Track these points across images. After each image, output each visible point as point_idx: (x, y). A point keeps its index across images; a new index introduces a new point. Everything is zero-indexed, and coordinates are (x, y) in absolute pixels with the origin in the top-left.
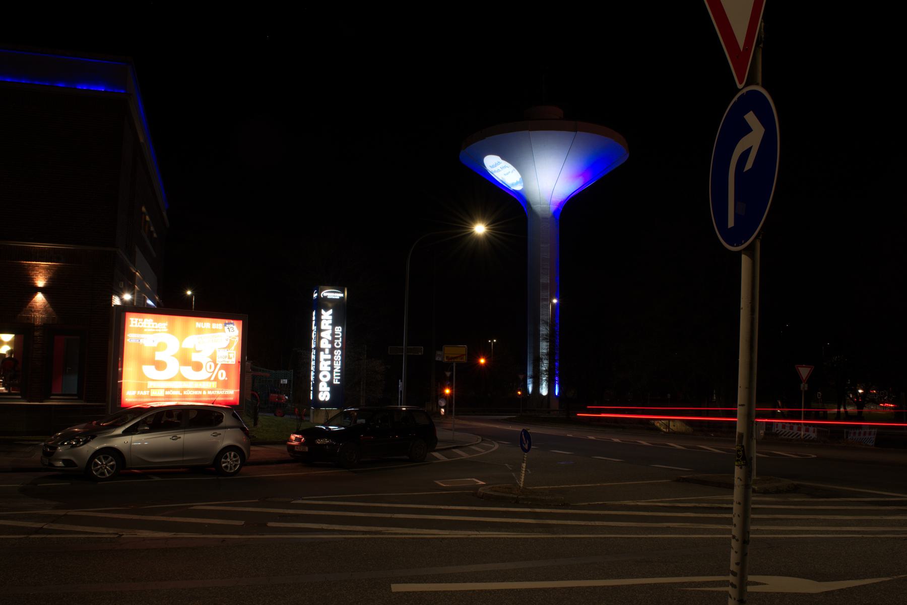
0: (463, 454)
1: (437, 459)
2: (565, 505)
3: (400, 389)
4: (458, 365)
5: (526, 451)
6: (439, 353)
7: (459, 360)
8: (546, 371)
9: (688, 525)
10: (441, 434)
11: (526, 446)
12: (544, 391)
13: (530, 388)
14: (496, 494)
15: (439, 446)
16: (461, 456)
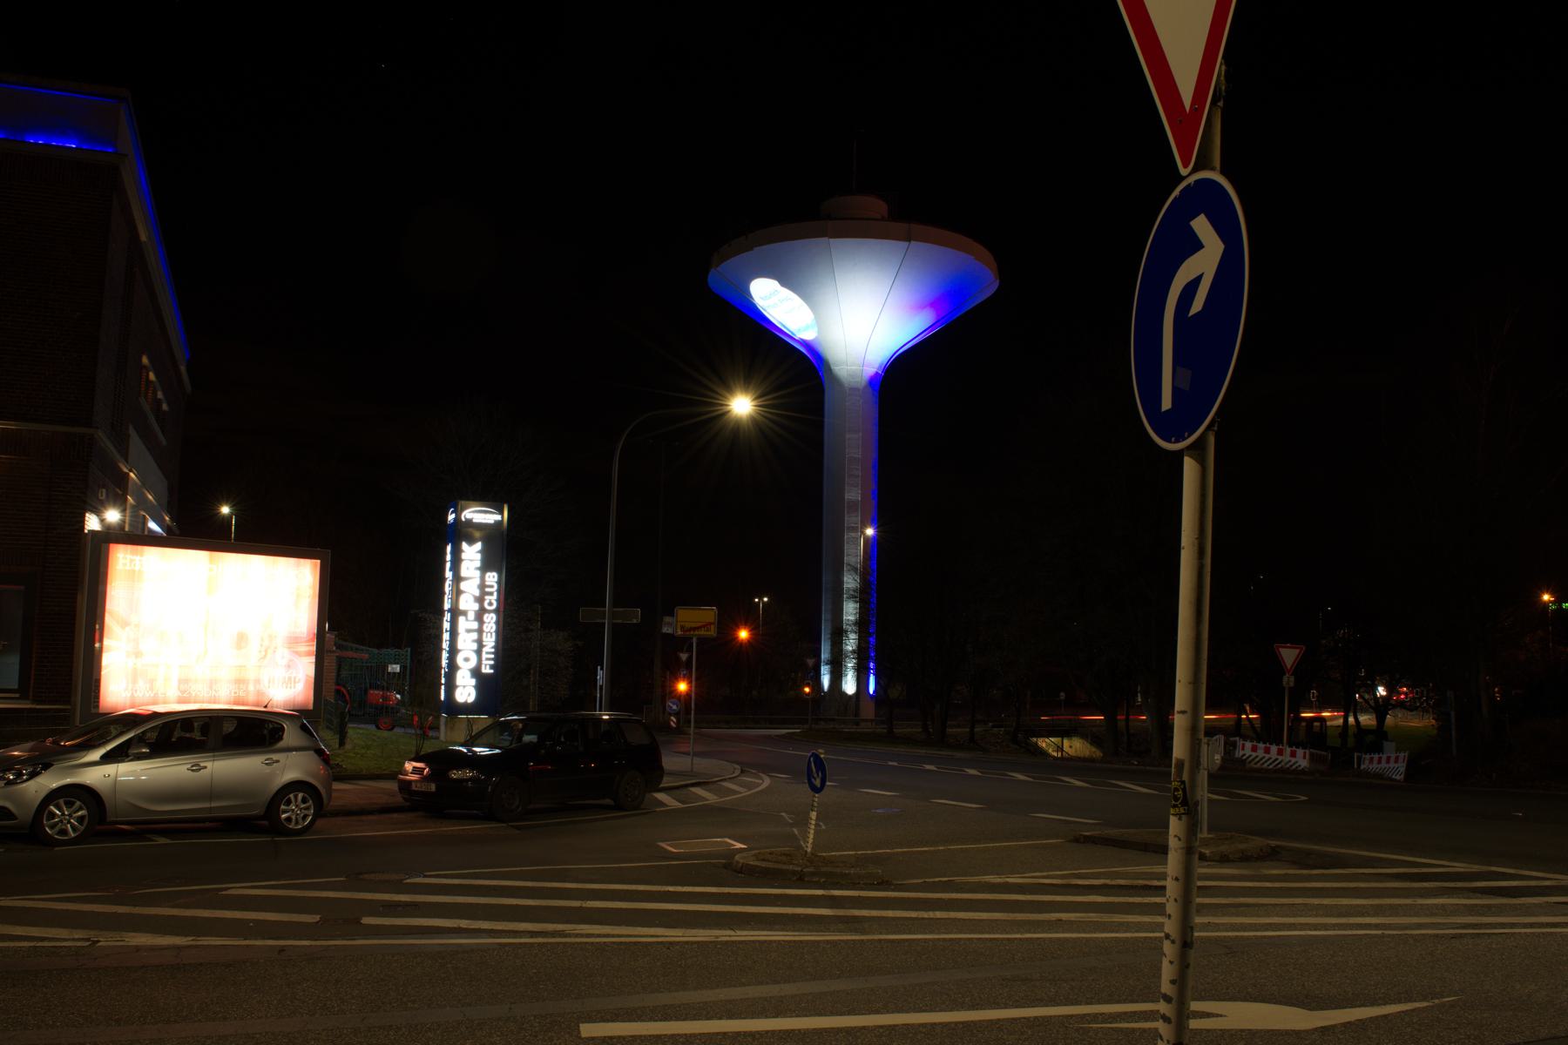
0: (708, 796)
1: (662, 804)
2: (883, 884)
3: (600, 682)
4: (702, 641)
5: (816, 790)
6: (667, 619)
7: (702, 632)
8: (853, 652)
9: (1093, 917)
10: (670, 761)
11: (818, 783)
12: (849, 686)
13: (826, 681)
14: (764, 864)
15: (666, 782)
16: (705, 799)
